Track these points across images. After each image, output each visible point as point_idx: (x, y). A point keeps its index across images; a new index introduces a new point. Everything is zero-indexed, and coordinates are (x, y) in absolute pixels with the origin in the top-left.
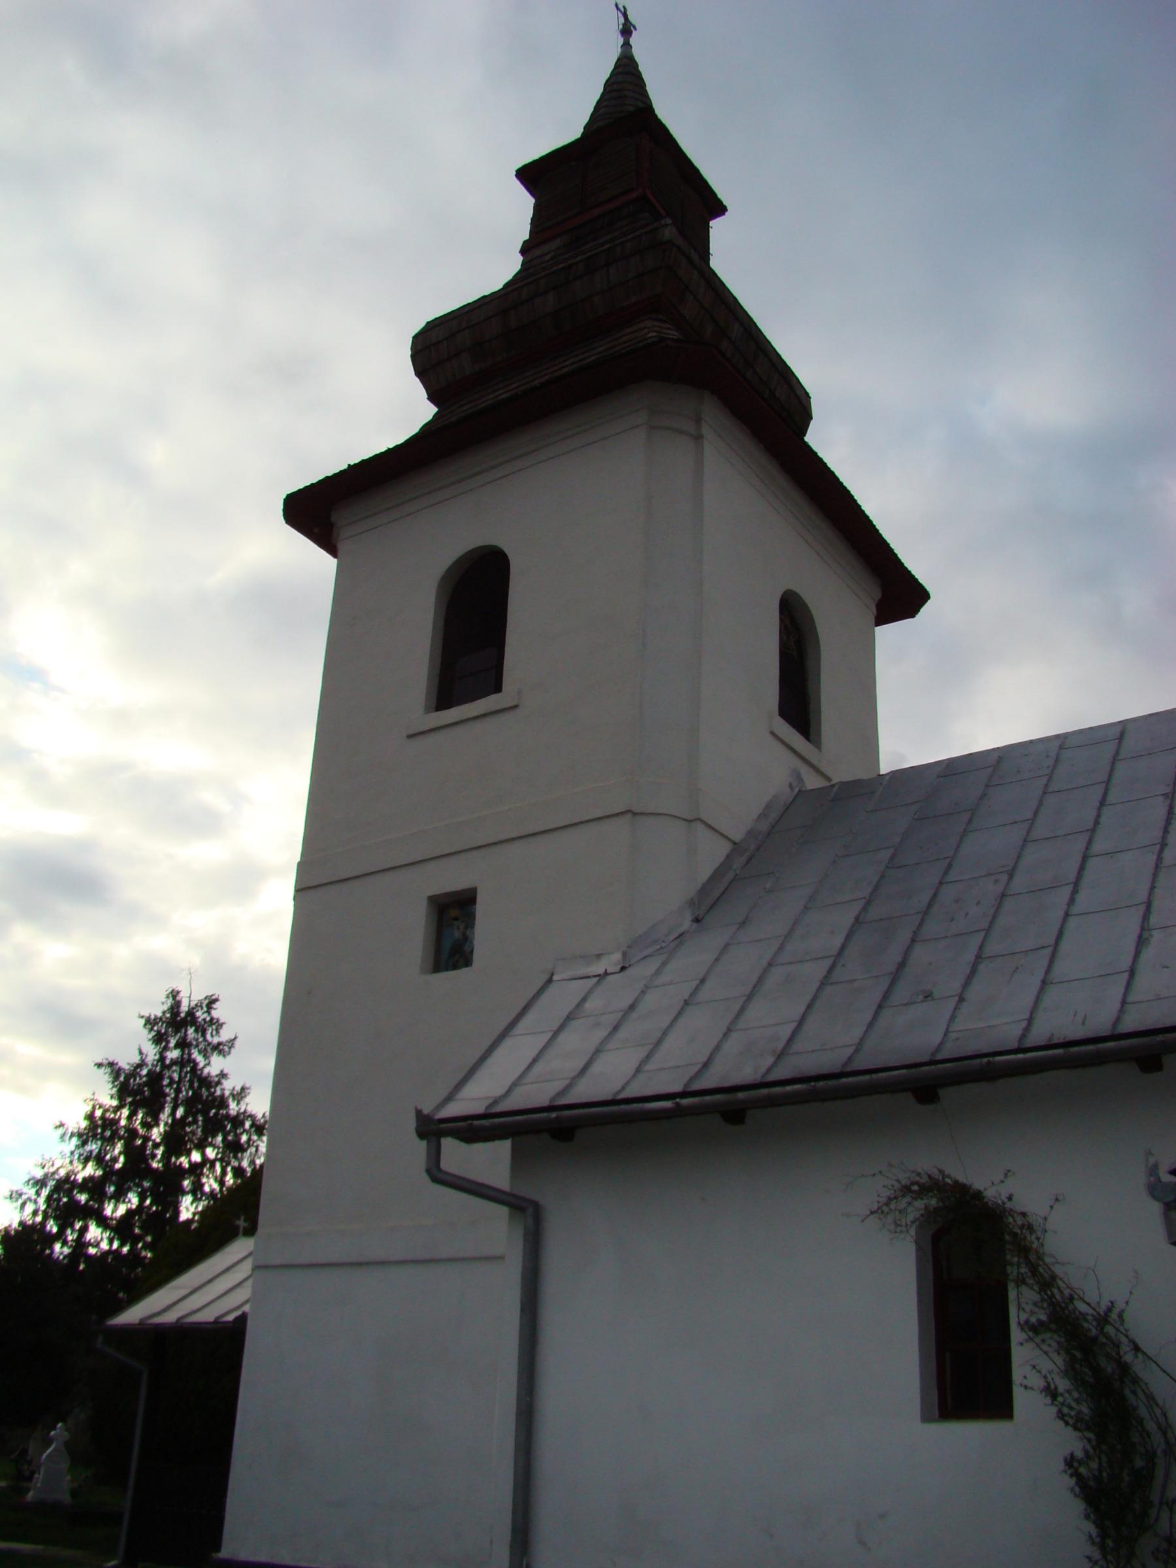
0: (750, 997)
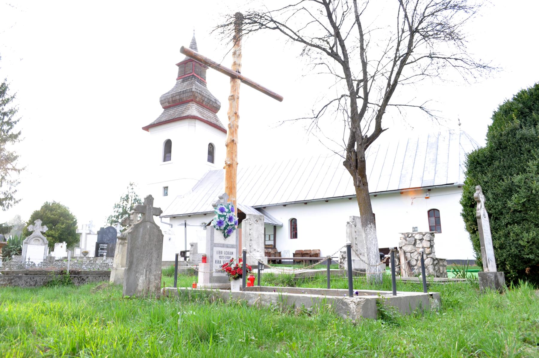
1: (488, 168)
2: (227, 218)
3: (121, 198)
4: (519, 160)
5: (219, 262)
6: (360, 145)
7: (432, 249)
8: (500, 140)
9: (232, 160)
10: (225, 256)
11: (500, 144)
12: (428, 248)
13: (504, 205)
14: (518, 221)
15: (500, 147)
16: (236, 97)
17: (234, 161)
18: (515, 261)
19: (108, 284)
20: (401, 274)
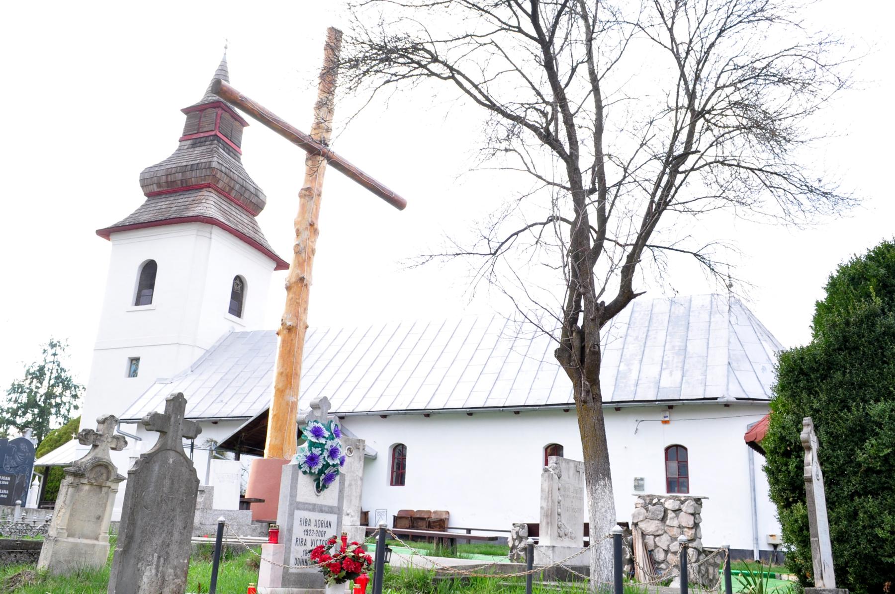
0: (192, 396)
1: (821, 384)
2: (327, 449)
3: (28, 371)
4: (879, 373)
5: (303, 543)
6: (592, 320)
7: (696, 530)
8: (845, 332)
9: (295, 318)
10: (315, 529)
11: (846, 339)
12: (689, 528)
13: (849, 457)
14: (874, 489)
15: (845, 345)
16: (315, 192)
17: (301, 320)
18: (865, 568)
19: (33, 572)
20: (636, 577)
